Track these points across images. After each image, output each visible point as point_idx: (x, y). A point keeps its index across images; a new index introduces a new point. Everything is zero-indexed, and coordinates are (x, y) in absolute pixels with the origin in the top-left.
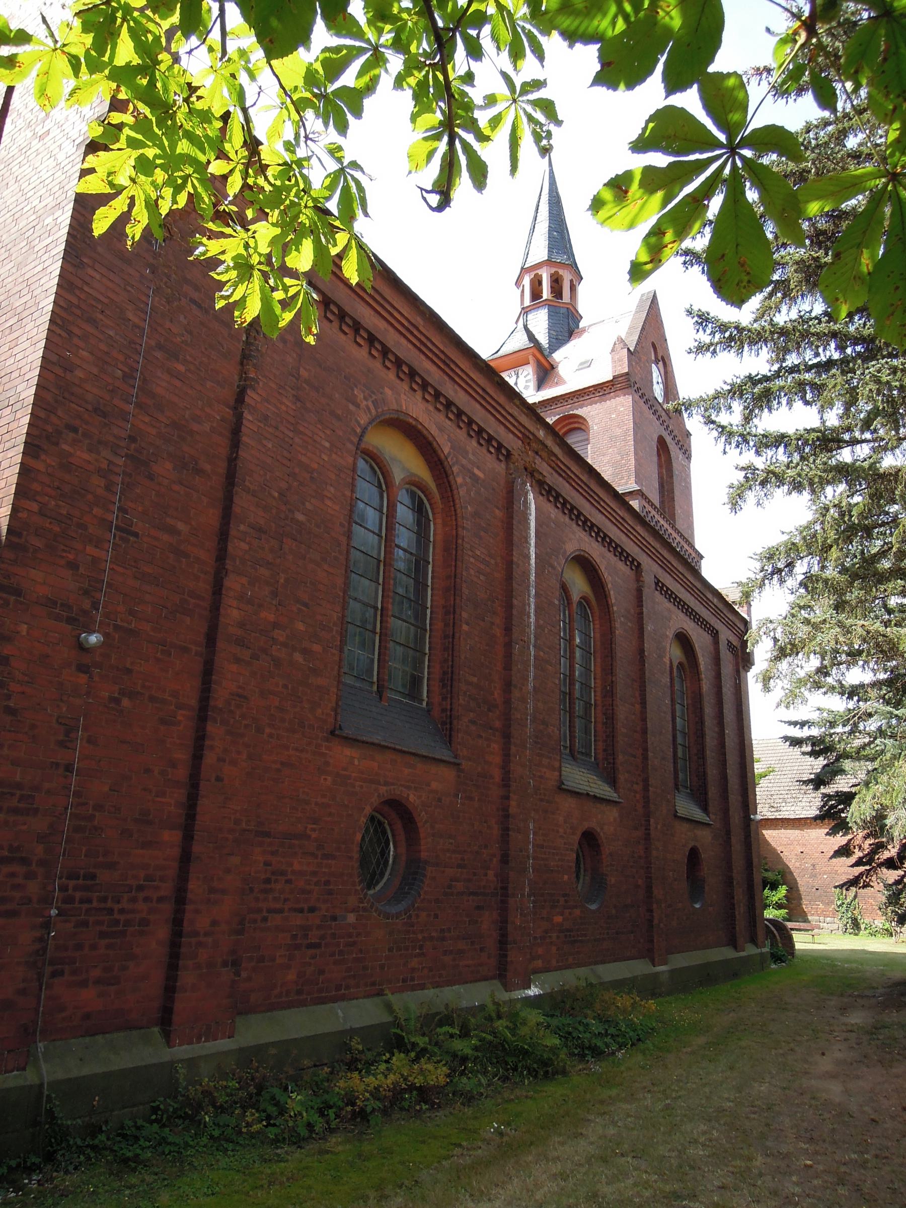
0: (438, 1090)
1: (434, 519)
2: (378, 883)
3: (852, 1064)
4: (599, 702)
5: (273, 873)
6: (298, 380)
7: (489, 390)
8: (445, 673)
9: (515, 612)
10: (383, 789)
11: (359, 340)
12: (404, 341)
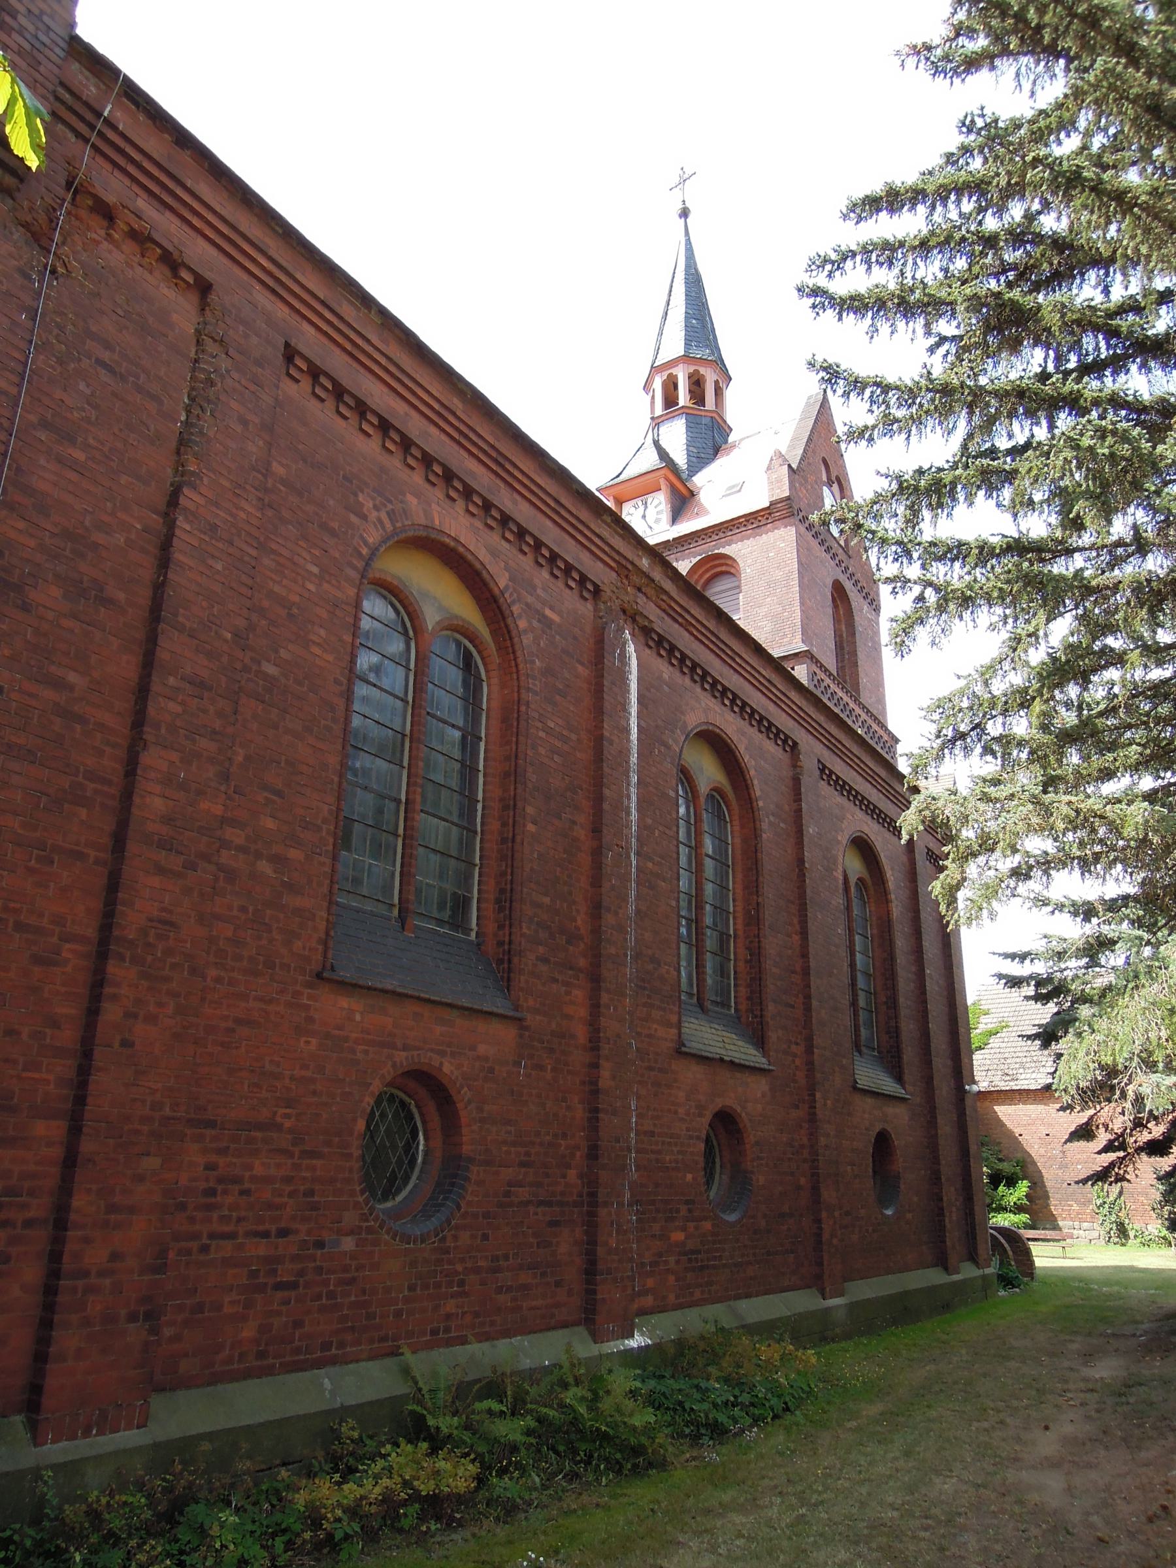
0: (460, 1500)
1: (488, 678)
2: (399, 1191)
3: (1084, 1444)
4: (740, 933)
5: (220, 1180)
6: (265, 476)
7: (563, 501)
8: (502, 891)
9: (606, 806)
10: (401, 1056)
11: (365, 426)
12: (433, 430)
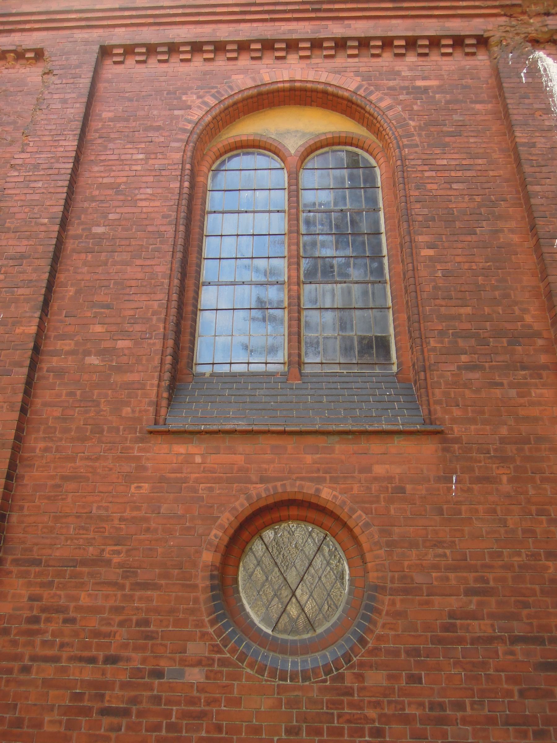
5: (44, 610)
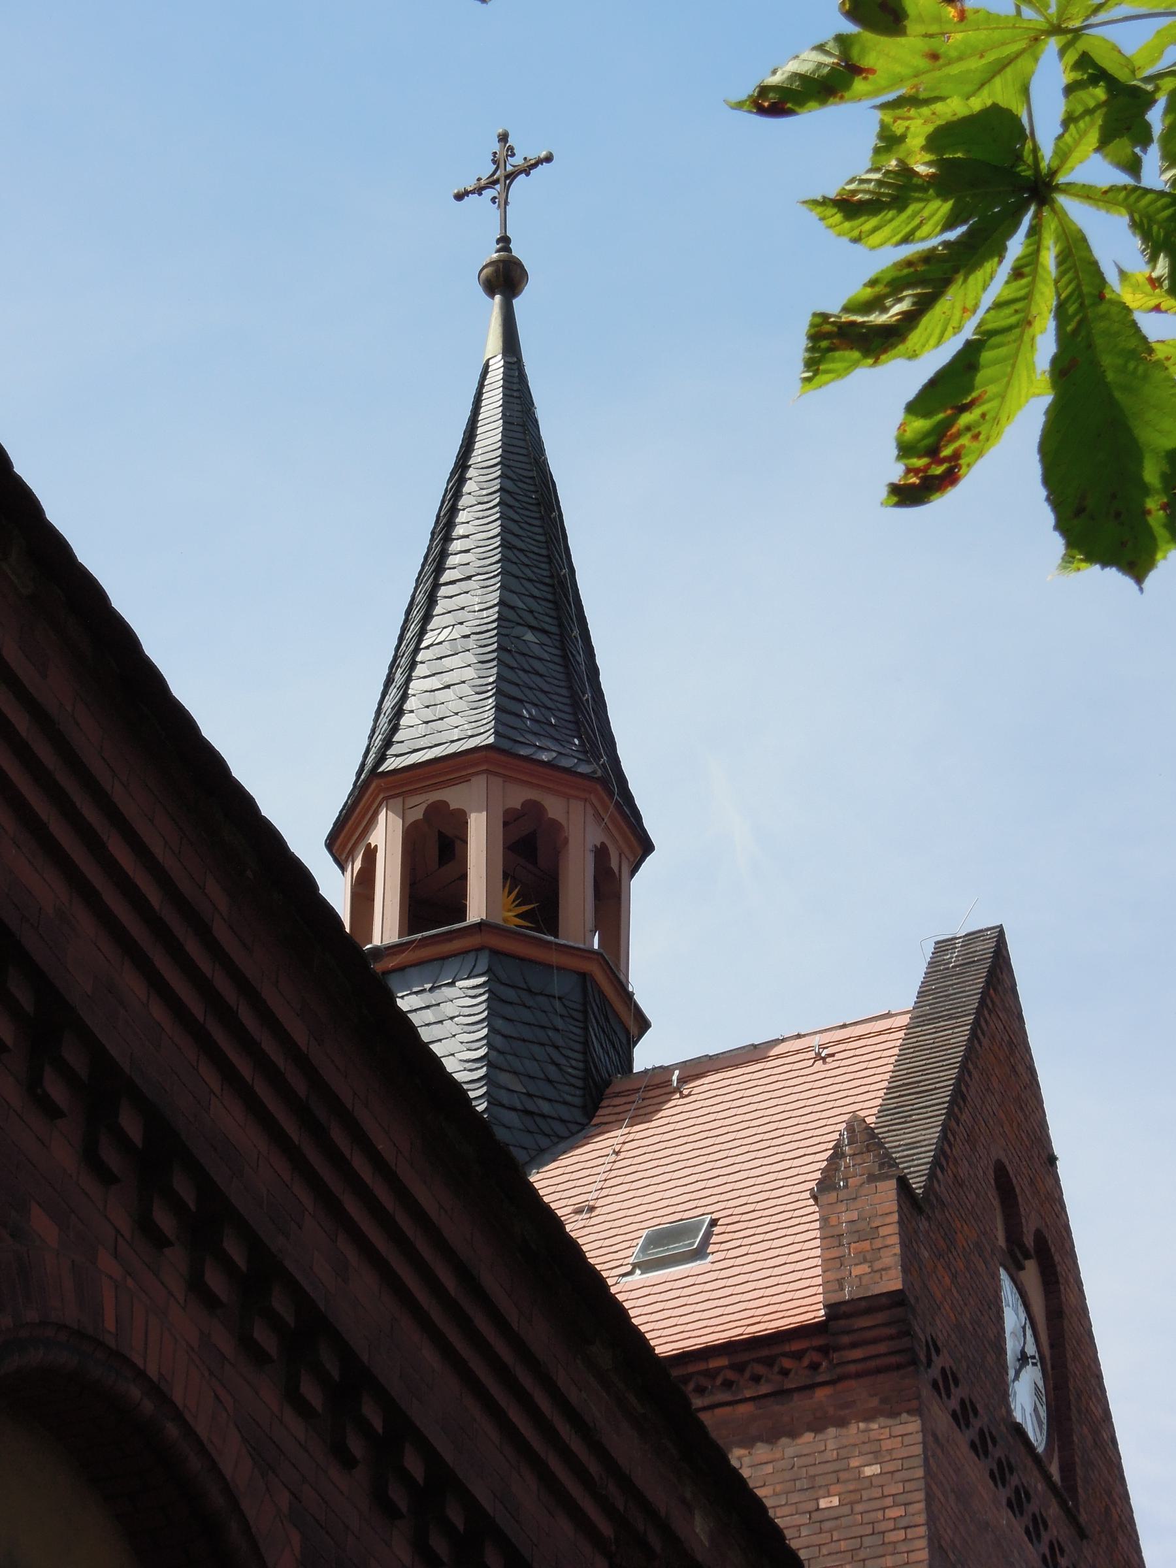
12: (133, 984)
